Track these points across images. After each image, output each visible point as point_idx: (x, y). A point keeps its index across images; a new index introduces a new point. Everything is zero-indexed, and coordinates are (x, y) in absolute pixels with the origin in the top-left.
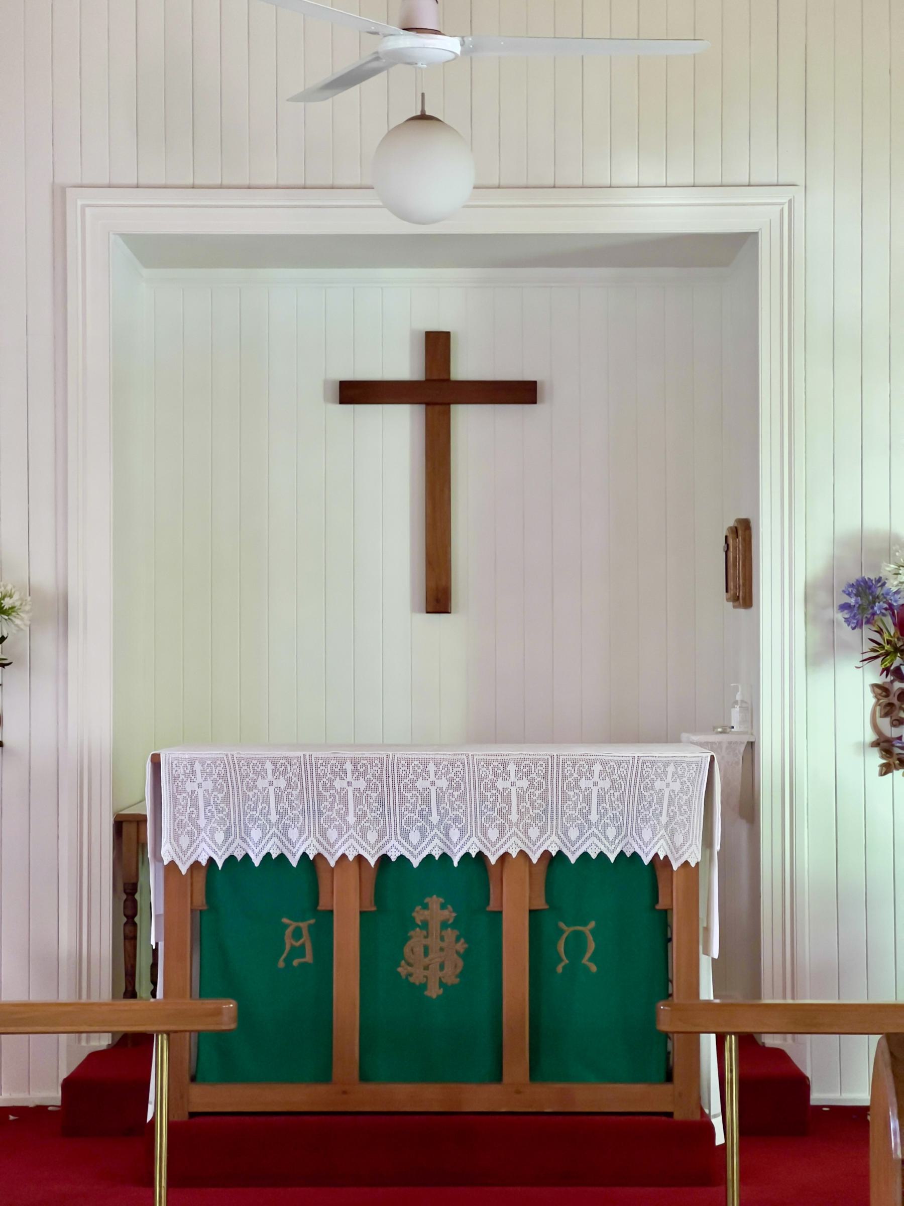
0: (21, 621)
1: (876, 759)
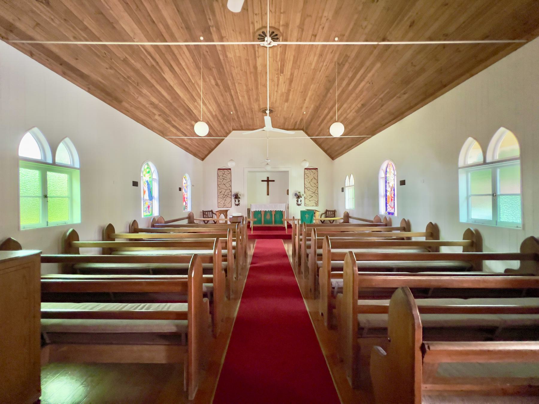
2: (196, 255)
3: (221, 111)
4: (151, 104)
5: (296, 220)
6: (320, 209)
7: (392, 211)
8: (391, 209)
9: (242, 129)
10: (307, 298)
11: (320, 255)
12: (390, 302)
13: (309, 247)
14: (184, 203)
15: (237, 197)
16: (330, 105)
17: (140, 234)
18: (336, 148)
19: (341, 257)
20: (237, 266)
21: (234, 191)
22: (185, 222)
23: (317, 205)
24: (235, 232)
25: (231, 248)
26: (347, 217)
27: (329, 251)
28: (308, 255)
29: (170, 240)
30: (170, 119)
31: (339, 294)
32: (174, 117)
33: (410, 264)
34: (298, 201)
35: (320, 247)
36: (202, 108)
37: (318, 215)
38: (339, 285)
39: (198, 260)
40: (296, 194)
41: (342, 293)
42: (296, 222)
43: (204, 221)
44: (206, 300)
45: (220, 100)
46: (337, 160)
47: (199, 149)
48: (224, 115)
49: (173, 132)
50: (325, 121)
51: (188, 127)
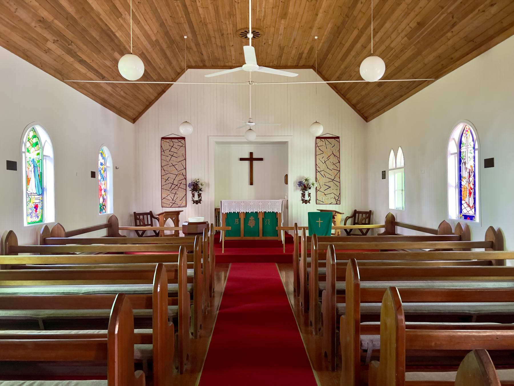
0: (204, 186)
1: (302, 202)
2: (122, 295)
3: (167, 34)
4: (40, 21)
5: (300, 228)
6: (344, 209)
7: (471, 213)
8: (468, 209)
9: (204, 67)
10: (320, 369)
11: (342, 292)
12: (457, 373)
13: (322, 278)
14: (101, 200)
15: (196, 187)
16: (360, 26)
17: (21, 256)
18: (373, 101)
19: (377, 295)
20: (196, 312)
21: (191, 177)
22: (102, 233)
23: (338, 201)
24: (192, 252)
25: (184, 280)
26: (392, 222)
27: (357, 286)
28: (320, 292)
29: (76, 266)
30: (73, 47)
31: (373, 362)
32: (81, 45)
33: (500, 308)
34: (303, 195)
35: (342, 278)
36: (132, 27)
37: (339, 218)
38: (374, 345)
39: (126, 304)
40: (300, 184)
41: (379, 360)
42: (300, 233)
43: (137, 231)
44: (139, 373)
45: (165, 15)
46: (374, 122)
47: (127, 102)
48: (172, 42)
49: (79, 72)
50: (353, 53)
51: (108, 63)
